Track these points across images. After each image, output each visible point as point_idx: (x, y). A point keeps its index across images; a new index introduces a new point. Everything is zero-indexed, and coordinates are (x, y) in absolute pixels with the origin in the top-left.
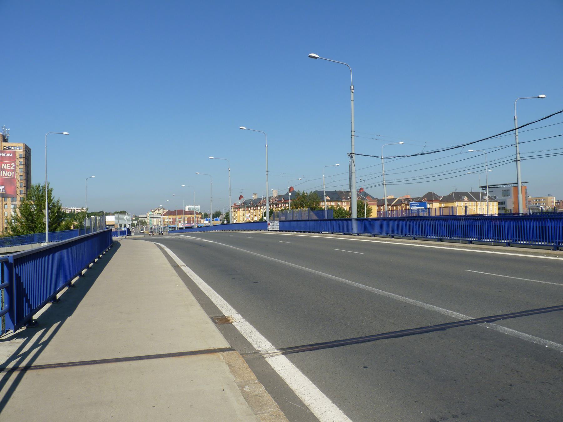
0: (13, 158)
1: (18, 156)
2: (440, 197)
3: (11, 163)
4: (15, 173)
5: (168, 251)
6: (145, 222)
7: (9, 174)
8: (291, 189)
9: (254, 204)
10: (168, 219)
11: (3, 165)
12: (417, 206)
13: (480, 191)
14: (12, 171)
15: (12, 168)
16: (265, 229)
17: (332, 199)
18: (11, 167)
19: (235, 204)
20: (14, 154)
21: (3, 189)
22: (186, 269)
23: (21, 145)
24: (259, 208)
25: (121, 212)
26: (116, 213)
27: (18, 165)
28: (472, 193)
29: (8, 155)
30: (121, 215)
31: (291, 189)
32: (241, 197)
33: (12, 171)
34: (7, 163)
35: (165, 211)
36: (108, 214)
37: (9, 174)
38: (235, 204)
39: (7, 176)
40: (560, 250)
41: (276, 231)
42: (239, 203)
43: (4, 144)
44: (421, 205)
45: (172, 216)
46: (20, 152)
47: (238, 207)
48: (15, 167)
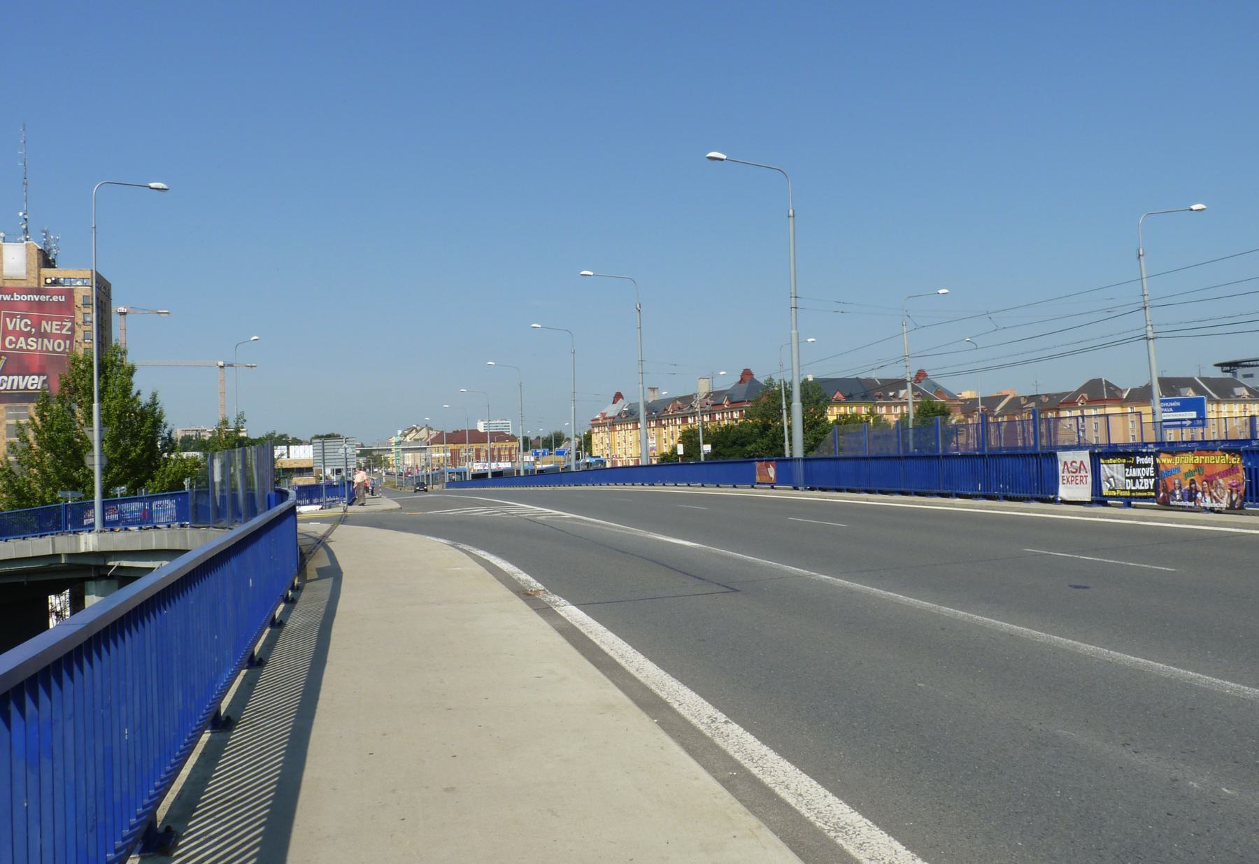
0: (67, 306)
1: (78, 300)
2: (1122, 391)
3: (61, 320)
4: (71, 344)
5: (481, 553)
6: (386, 459)
7: (59, 346)
8: (747, 374)
9: (658, 413)
10: (439, 454)
11: (44, 323)
12: (1176, 409)
13: (1218, 373)
14: (65, 337)
15: (64, 332)
16: (1045, 490)
17: (850, 399)
18: (62, 327)
19: (603, 415)
20: (70, 294)
21: (44, 382)
22: (739, 741)
23: (87, 274)
24: (618, 428)
25: (329, 437)
26: (318, 437)
27: (80, 322)
28: (1204, 380)
29: (55, 298)
30: (329, 444)
31: (747, 374)
32: (618, 396)
33: (65, 337)
34: (52, 319)
35: (434, 434)
36: (297, 442)
37: (59, 346)
38: (603, 415)
39: (54, 351)
40: (1135, 507)
41: (1219, 512)
42: (612, 410)
43: (46, 272)
44: (1186, 405)
45: (452, 446)
46: (84, 291)
47: (612, 423)
48: (72, 329)
